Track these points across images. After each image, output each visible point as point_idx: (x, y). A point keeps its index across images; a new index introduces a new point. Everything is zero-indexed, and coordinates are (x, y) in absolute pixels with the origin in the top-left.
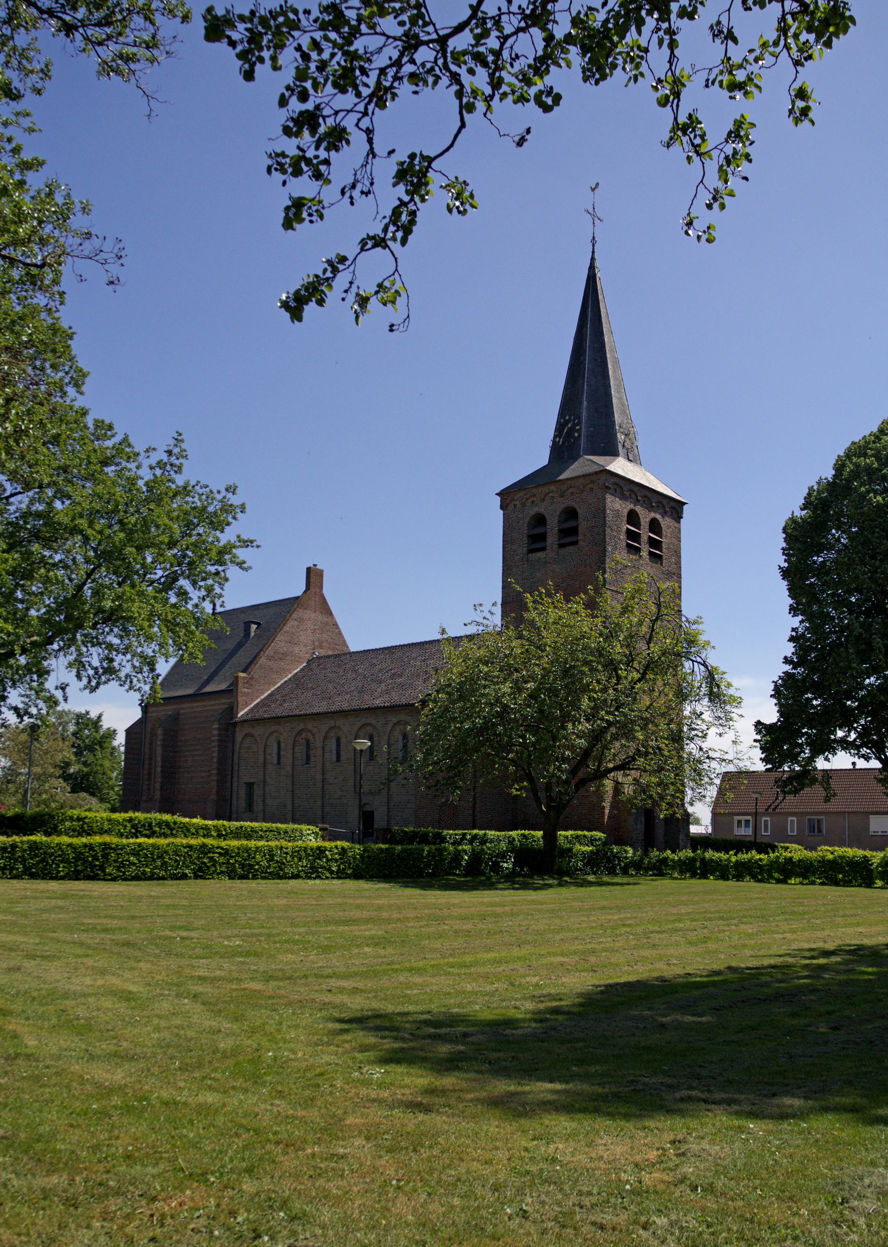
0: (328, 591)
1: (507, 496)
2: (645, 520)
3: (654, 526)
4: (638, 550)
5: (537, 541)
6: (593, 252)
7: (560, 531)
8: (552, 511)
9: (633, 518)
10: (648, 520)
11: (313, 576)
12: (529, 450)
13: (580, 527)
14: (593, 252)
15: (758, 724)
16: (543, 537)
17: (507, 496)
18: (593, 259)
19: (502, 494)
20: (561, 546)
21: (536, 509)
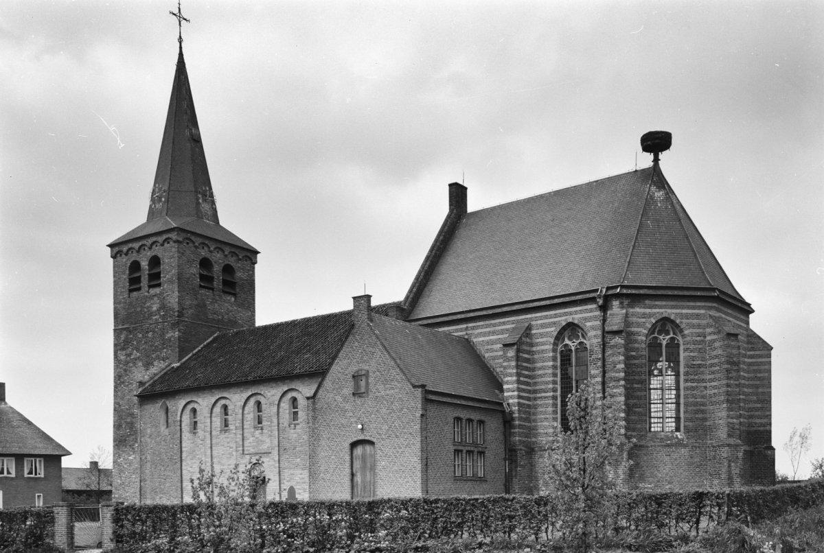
3: (228, 269)
6: (181, 48)
12: (132, 212)
14: (181, 48)
17: (117, 248)
18: (181, 55)
20: (150, 287)
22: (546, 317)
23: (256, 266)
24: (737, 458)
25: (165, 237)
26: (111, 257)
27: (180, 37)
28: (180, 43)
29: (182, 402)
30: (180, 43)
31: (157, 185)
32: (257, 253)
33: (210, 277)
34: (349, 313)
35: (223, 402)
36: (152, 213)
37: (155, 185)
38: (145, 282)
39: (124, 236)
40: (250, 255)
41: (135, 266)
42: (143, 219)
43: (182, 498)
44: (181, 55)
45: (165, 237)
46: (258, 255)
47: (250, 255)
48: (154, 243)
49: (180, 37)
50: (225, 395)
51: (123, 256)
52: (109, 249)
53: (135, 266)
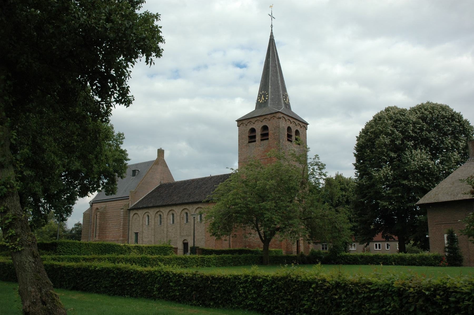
3: (297, 132)
5: (252, 138)
7: (261, 134)
8: (258, 127)
9: (289, 129)
10: (295, 130)
16: (254, 137)
35: (186, 211)
36: (259, 105)
38: (258, 138)
41: (253, 130)
44: (272, 33)
53: (253, 130)
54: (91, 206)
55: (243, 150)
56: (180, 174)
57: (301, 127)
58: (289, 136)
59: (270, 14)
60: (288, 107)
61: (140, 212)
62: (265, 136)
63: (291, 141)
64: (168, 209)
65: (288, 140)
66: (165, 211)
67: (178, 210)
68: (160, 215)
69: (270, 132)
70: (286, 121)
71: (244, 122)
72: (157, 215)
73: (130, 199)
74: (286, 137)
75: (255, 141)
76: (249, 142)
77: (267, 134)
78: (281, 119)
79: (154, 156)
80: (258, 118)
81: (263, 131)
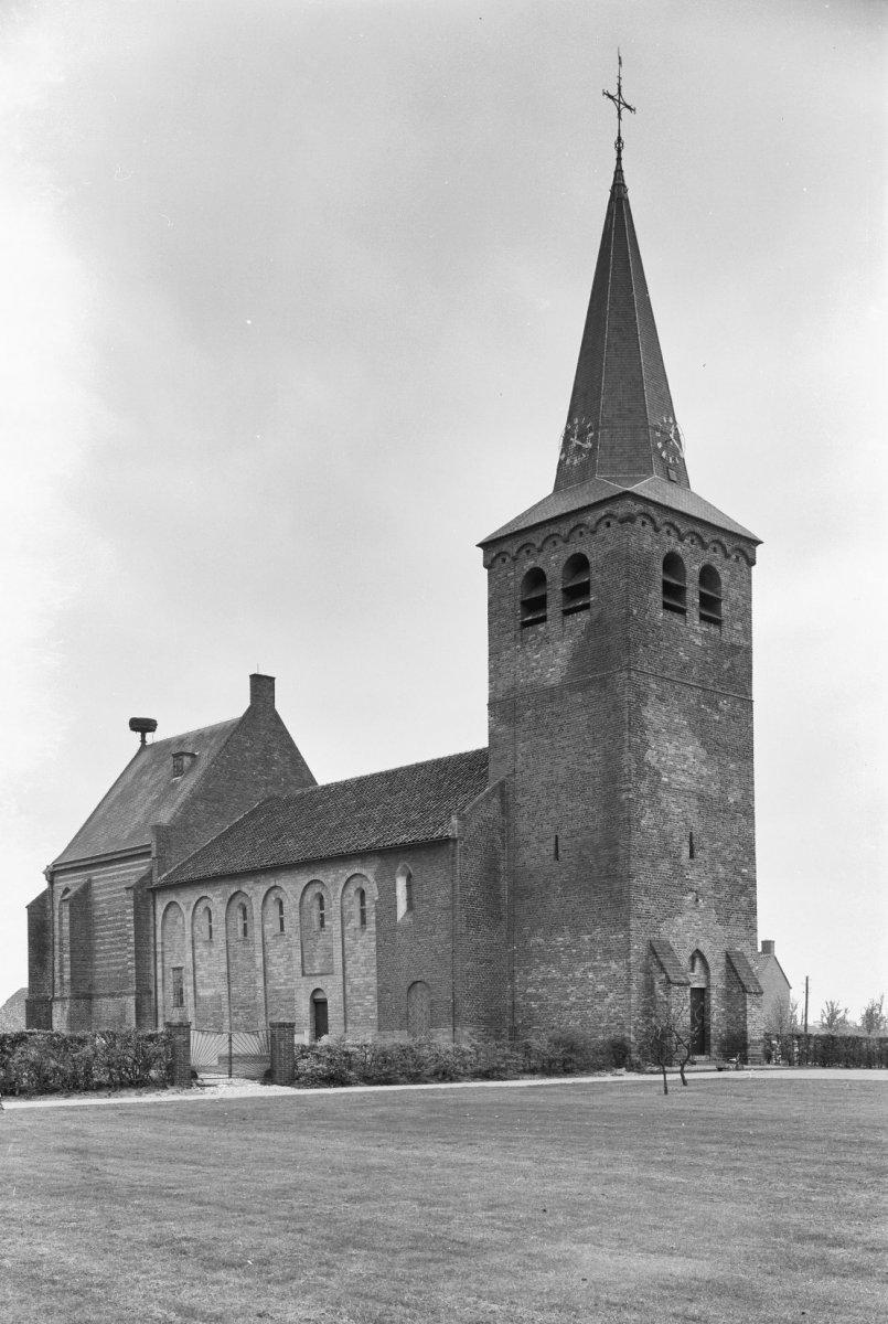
0: (281, 706)
1: (495, 549)
2: (693, 569)
3: (708, 576)
4: (682, 612)
5: (534, 607)
6: (619, 159)
7: (565, 591)
8: (553, 563)
9: (672, 563)
10: (697, 568)
11: (262, 686)
12: (521, 475)
13: (592, 583)
14: (619, 159)
15: (761, 542)
16: (540, 603)
17: (495, 549)
18: (619, 172)
19: (274, 679)
20: (567, 613)
21: (531, 563)
22: (134, 866)
23: (753, 568)
24: (350, 1068)
25: (572, 524)
26: (485, 566)
27: (619, 139)
28: (619, 151)
29: (262, 889)
30: (619, 151)
31: (576, 421)
32: (274, 679)
33: (678, 587)
34: (480, 753)
35: (316, 889)
36: (566, 477)
37: (570, 420)
38: (554, 607)
39: (508, 525)
40: (743, 547)
41: (537, 578)
42: (547, 488)
43: (231, 1048)
44: (619, 172)
45: (572, 524)
46: (759, 549)
47: (743, 547)
48: (610, 515)
49: (619, 139)
50: (317, 877)
51: (560, 544)
52: (481, 551)
53: (537, 578)
54: (51, 882)
55: (506, 655)
56: (331, 758)
57: (681, 539)
58: (673, 592)
59: (614, 92)
60: (673, 474)
61: (186, 899)
62: (577, 593)
63: (682, 612)
64: (303, 879)
65: (666, 606)
66: (255, 890)
67: (291, 887)
68: (207, 909)
69: (595, 577)
70: (657, 530)
71: (504, 547)
72: (352, 890)
73: (154, 855)
74: (656, 596)
75: (543, 619)
76: (525, 625)
77: (584, 589)
78: (638, 524)
79: (237, 704)
80: (553, 529)
81: (588, 583)
